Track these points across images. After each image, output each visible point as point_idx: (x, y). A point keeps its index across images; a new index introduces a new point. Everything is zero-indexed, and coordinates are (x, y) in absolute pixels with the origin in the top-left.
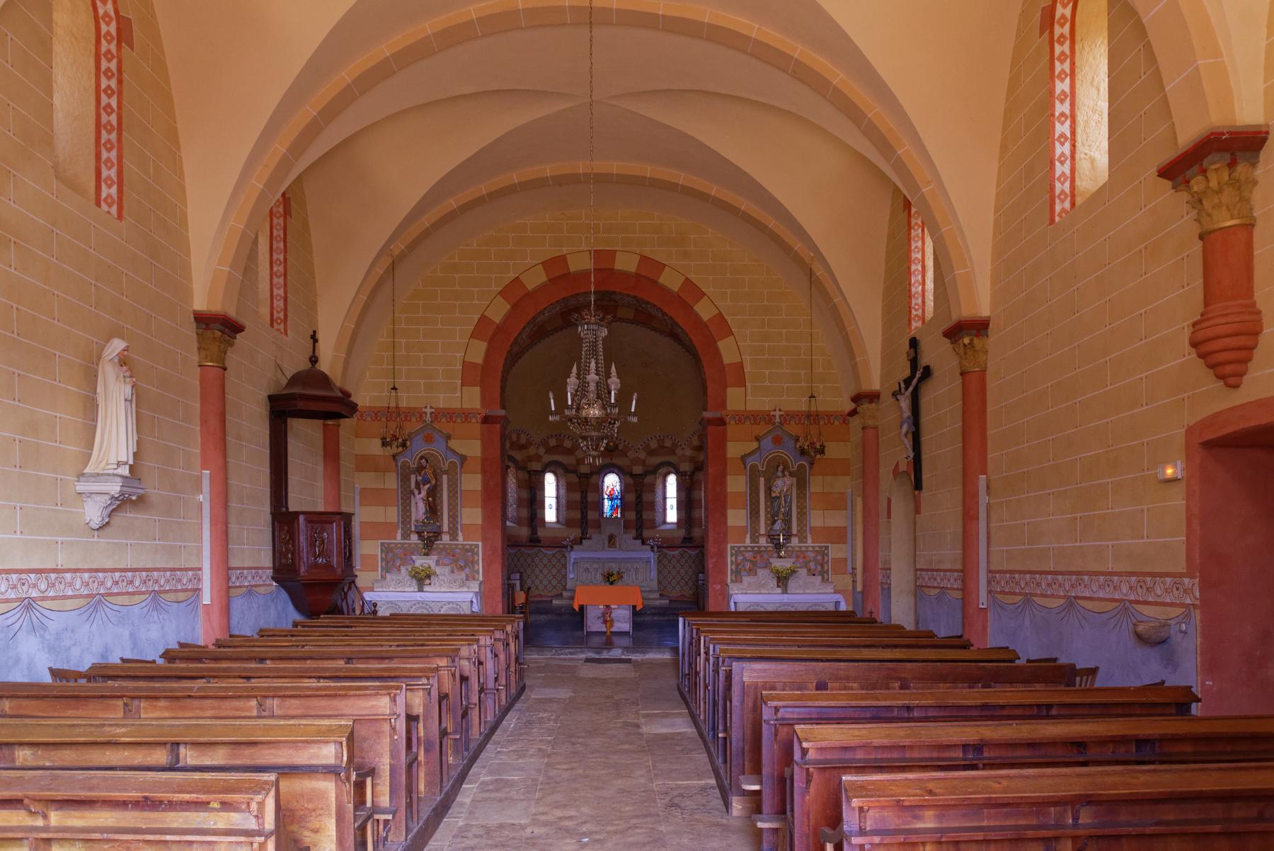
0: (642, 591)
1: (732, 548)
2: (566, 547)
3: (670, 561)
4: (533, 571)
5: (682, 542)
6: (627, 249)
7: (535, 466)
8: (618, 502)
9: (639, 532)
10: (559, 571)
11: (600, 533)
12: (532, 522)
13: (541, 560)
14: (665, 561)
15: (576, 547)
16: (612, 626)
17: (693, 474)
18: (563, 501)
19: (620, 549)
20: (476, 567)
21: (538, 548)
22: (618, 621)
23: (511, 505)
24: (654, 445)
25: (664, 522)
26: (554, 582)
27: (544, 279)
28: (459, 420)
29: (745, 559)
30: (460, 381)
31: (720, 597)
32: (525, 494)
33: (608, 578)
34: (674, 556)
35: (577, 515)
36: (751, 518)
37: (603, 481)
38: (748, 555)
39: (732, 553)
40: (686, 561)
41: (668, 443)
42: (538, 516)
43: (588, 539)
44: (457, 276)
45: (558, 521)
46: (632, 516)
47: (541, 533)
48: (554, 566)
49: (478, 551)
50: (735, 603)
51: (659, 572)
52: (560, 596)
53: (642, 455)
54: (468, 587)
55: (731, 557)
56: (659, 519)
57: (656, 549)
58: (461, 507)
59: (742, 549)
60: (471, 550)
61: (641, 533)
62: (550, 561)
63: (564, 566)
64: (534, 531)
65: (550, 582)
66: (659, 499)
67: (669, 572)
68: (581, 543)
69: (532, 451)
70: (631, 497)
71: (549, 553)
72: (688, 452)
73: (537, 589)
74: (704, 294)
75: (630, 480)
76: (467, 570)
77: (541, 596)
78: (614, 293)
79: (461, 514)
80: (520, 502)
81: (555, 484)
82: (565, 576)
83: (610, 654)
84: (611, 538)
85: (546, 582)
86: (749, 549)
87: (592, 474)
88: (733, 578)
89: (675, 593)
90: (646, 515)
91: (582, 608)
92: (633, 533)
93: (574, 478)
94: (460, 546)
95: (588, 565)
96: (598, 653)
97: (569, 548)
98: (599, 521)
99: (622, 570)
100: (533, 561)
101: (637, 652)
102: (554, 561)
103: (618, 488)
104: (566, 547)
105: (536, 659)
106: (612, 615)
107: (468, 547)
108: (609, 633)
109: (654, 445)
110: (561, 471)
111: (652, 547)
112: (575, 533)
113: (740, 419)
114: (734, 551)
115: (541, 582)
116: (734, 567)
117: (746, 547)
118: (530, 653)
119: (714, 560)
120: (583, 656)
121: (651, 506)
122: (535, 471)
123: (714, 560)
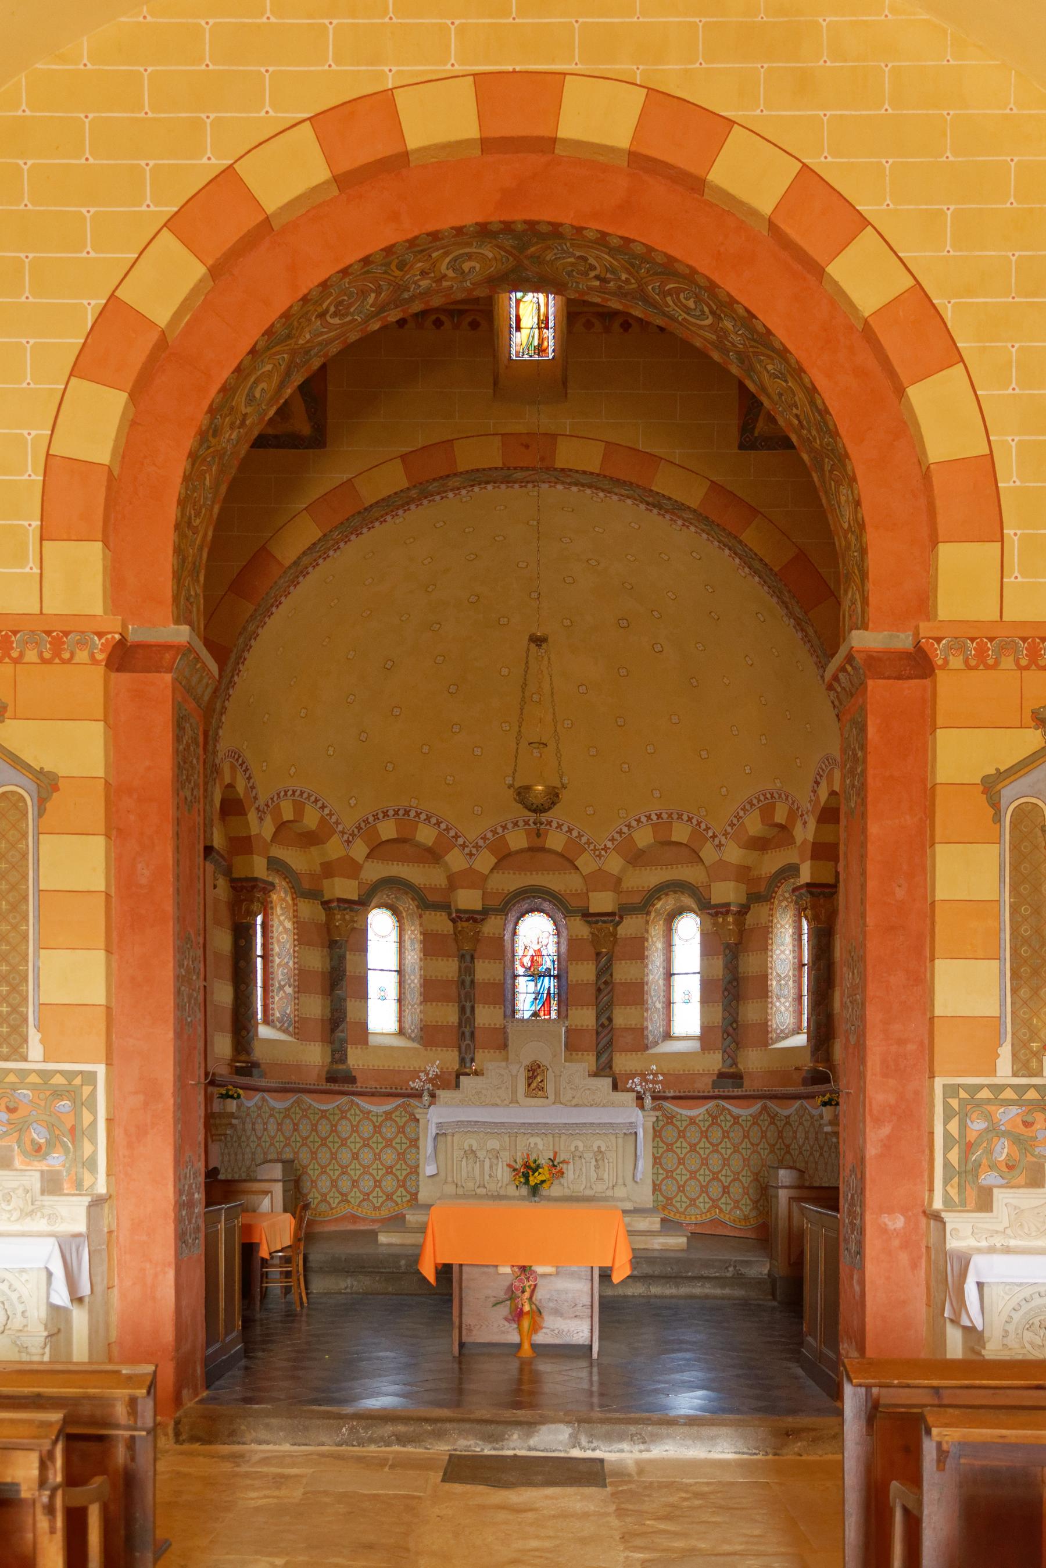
0: (631, 1233)
1: (951, 1091)
2: (417, 1095)
3: (682, 1134)
4: (334, 1156)
5: (715, 1085)
6: (602, 68)
7: (343, 888)
8: (549, 984)
9: (604, 1058)
10: (401, 1156)
11: (507, 1059)
12: (333, 1031)
13: (355, 1129)
14: (670, 1133)
15: (443, 1094)
16: (535, 1328)
17: (744, 910)
18: (414, 981)
19: (557, 1101)
20: (87, 1148)
21: (345, 1099)
22: (557, 1312)
23: (281, 988)
24: (644, 838)
25: (668, 1036)
26: (389, 1184)
27: (319, 172)
28: (31, 656)
29: (993, 1130)
30: (36, 523)
31: (904, 1258)
32: (317, 960)
33: (526, 1176)
34: (692, 1121)
35: (449, 1015)
36: (1014, 991)
37: (514, 933)
38: (1007, 1116)
39: (946, 1106)
40: (726, 1135)
41: (681, 833)
42: (351, 1015)
43: (476, 1073)
44: (26, 164)
45: (401, 1032)
46: (585, 1017)
47: (356, 1059)
48: (389, 1143)
49: (93, 1094)
50: (980, 1285)
51: (657, 1161)
52: (397, 1221)
53: (614, 864)
54: (52, 1218)
55: (946, 1121)
56: (654, 1025)
57: (648, 1101)
58: (39, 947)
59: (985, 1094)
60: (68, 1092)
61: (610, 1061)
62: (377, 1129)
63: (414, 1143)
64: (339, 1055)
65: (377, 1183)
66: (655, 974)
67: (681, 1161)
68: (457, 1086)
69: (334, 849)
70: (585, 972)
71: (374, 1108)
72: (734, 854)
73: (345, 1198)
74: (865, 222)
75: (583, 930)
76: (56, 1160)
77: (354, 1218)
78: (556, 231)
79: (37, 970)
80: (302, 980)
81: (394, 936)
82: (415, 1170)
83: (532, 1442)
84: (534, 1072)
85: (367, 1184)
86: (1008, 1094)
87: (485, 913)
88: (953, 1192)
89: (697, 1214)
90: (622, 1017)
91: (445, 1272)
92: (588, 1061)
93: (441, 923)
94: (33, 1078)
95: (472, 1142)
96: (491, 1438)
97: (426, 1097)
98: (503, 1031)
99: (562, 1157)
100: (334, 1129)
101: (621, 1438)
102: (389, 1131)
103: (552, 949)
104: (417, 1095)
105: (281, 1459)
106: (539, 1295)
107: (59, 1080)
108: (526, 1351)
109: (644, 838)
110: (407, 904)
111: (640, 1098)
112: (446, 1059)
113: (981, 652)
114: (954, 1103)
115: (355, 1183)
116: (954, 1156)
117: (1001, 1088)
118: (263, 1434)
119: (886, 1130)
120: (442, 1449)
121: (637, 992)
122: (340, 900)
123: (886, 1130)
